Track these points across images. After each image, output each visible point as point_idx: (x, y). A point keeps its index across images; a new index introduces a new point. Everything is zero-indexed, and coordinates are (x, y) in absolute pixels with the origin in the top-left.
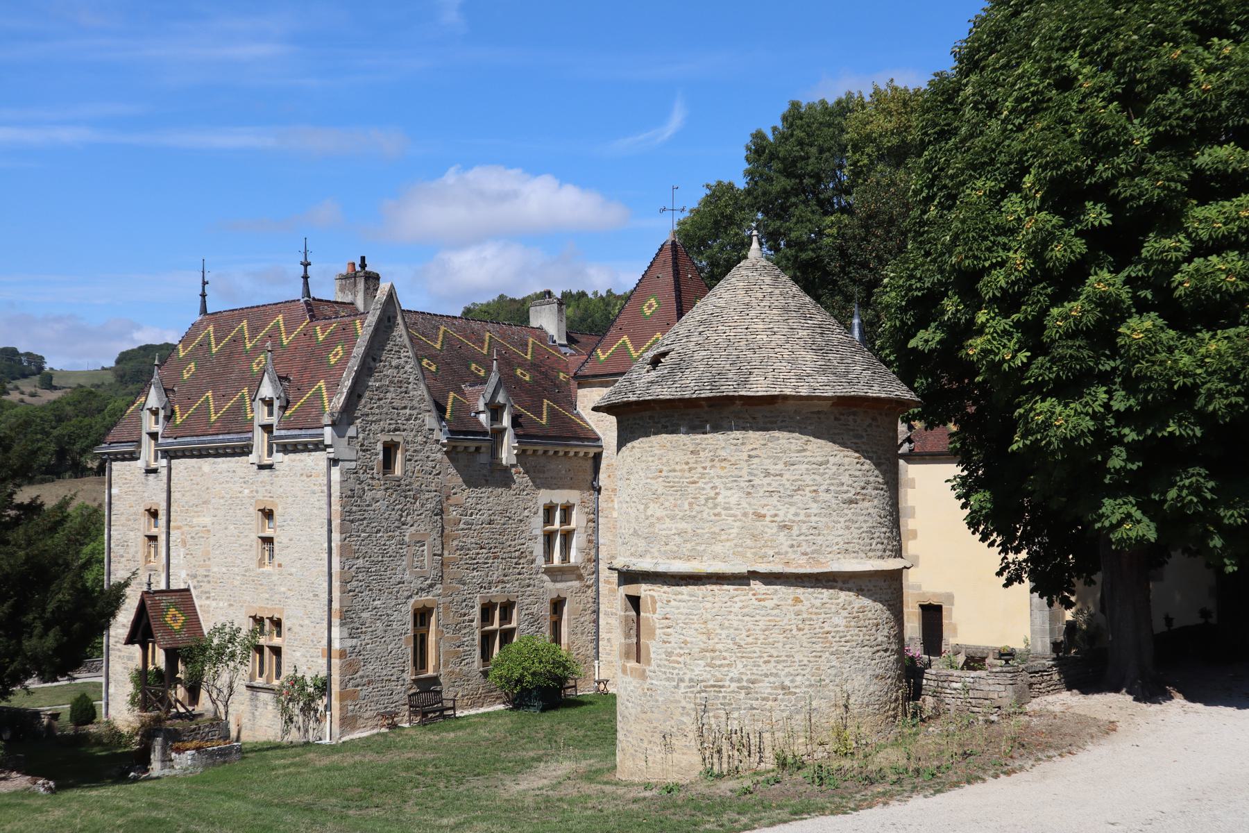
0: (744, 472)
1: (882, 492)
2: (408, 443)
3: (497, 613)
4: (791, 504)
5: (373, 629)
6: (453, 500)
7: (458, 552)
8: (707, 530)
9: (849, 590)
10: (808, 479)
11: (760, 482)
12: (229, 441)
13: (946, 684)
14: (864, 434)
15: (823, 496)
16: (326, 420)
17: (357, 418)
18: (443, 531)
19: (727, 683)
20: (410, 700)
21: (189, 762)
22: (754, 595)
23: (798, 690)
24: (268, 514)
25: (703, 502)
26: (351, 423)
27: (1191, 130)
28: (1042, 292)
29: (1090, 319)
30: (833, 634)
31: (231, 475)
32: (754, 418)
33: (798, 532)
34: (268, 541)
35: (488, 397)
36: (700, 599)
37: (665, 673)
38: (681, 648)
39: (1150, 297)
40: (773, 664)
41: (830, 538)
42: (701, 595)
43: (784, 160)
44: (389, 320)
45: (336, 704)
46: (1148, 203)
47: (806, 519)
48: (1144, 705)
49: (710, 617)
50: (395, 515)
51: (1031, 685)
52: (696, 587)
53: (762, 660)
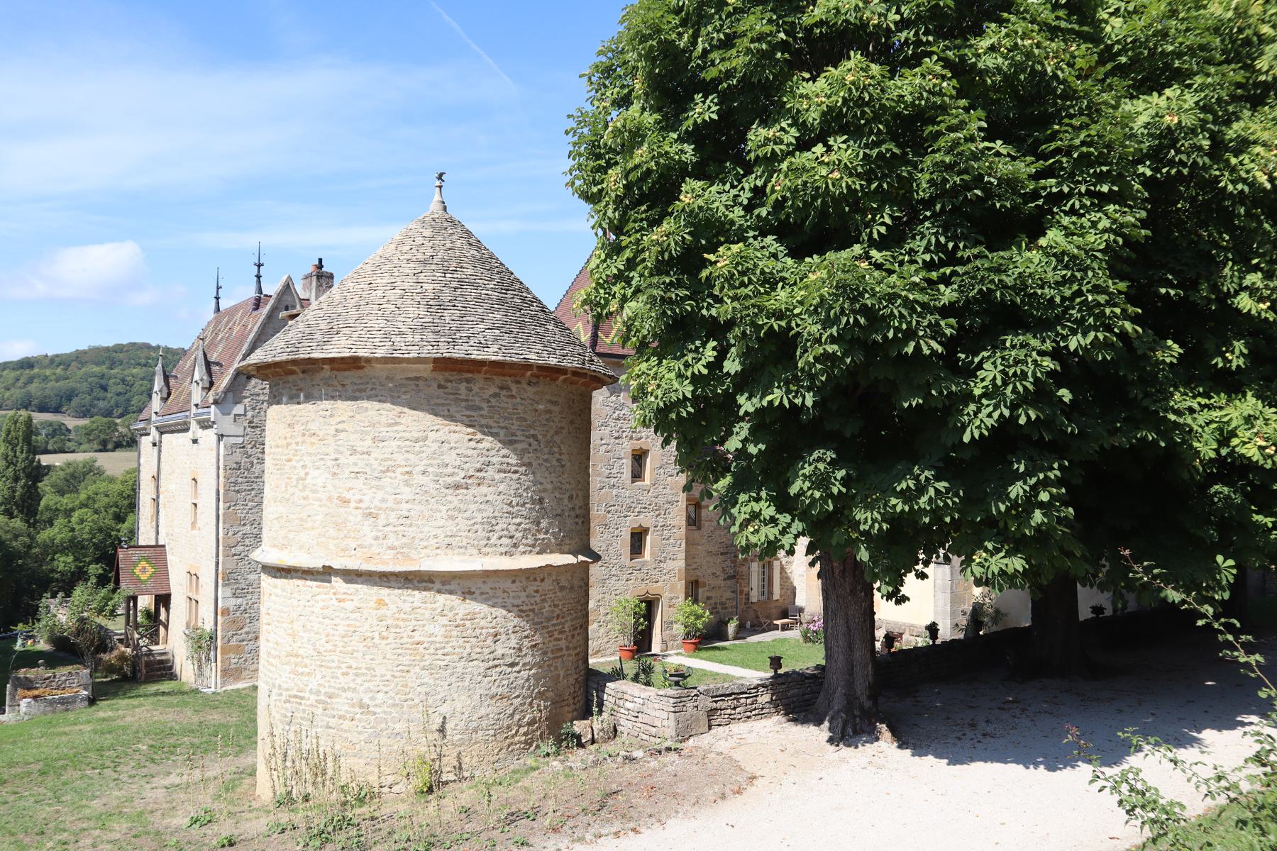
0: (331, 450)
1: (516, 476)
4: (378, 487)
9: (451, 593)
10: (400, 459)
11: (346, 461)
13: (621, 702)
14: (484, 405)
17: (246, 397)
19: (307, 695)
22: (334, 594)
23: (378, 710)
25: (295, 483)
30: (425, 645)
33: (385, 522)
40: (351, 677)
47: (397, 507)
53: (341, 671)
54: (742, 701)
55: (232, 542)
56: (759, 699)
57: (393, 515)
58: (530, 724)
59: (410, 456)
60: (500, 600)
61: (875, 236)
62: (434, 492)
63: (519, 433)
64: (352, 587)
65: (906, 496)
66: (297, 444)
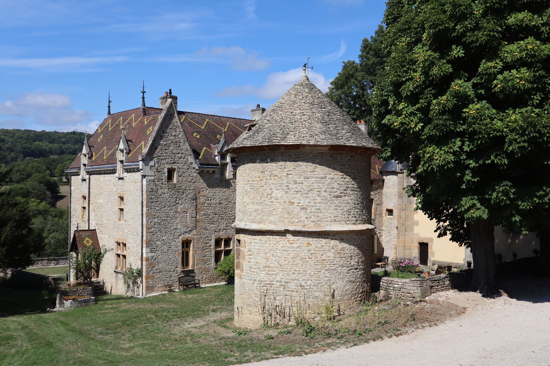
0: (285, 182)
1: (356, 192)
2: (180, 168)
3: (223, 243)
4: (307, 197)
5: (162, 249)
6: (202, 194)
7: (204, 216)
8: (267, 210)
9: (336, 240)
10: (316, 185)
11: (292, 187)
12: (108, 167)
13: (391, 285)
14: (346, 164)
15: (323, 194)
16: (140, 158)
17: (155, 158)
18: (196, 207)
19: (275, 283)
20: (179, 280)
21: (69, 305)
22: (288, 241)
24: (122, 198)
25: (266, 196)
26: (151, 160)
27: (505, 5)
28: (429, 92)
29: (450, 105)
31: (109, 182)
32: (290, 156)
33: (310, 211)
34: (122, 210)
35: (219, 149)
36: (264, 242)
37: (249, 276)
38: (255, 265)
39: (483, 93)
40: (296, 274)
41: (326, 214)
42: (264, 241)
43: (374, 50)
44: (171, 115)
45: (144, 280)
46: (481, 45)
48: (486, 299)
49: (268, 251)
50: (174, 200)
51: (431, 287)
52: (262, 237)
53: (291, 272)
54: (440, 283)
55: (150, 226)
56: (446, 283)
57: (313, 208)
58: (361, 293)
59: (320, 184)
60: (352, 243)
61: (535, 104)
62: (329, 199)
63: (357, 175)
64: (296, 238)
65: (539, 197)
66: (267, 180)
